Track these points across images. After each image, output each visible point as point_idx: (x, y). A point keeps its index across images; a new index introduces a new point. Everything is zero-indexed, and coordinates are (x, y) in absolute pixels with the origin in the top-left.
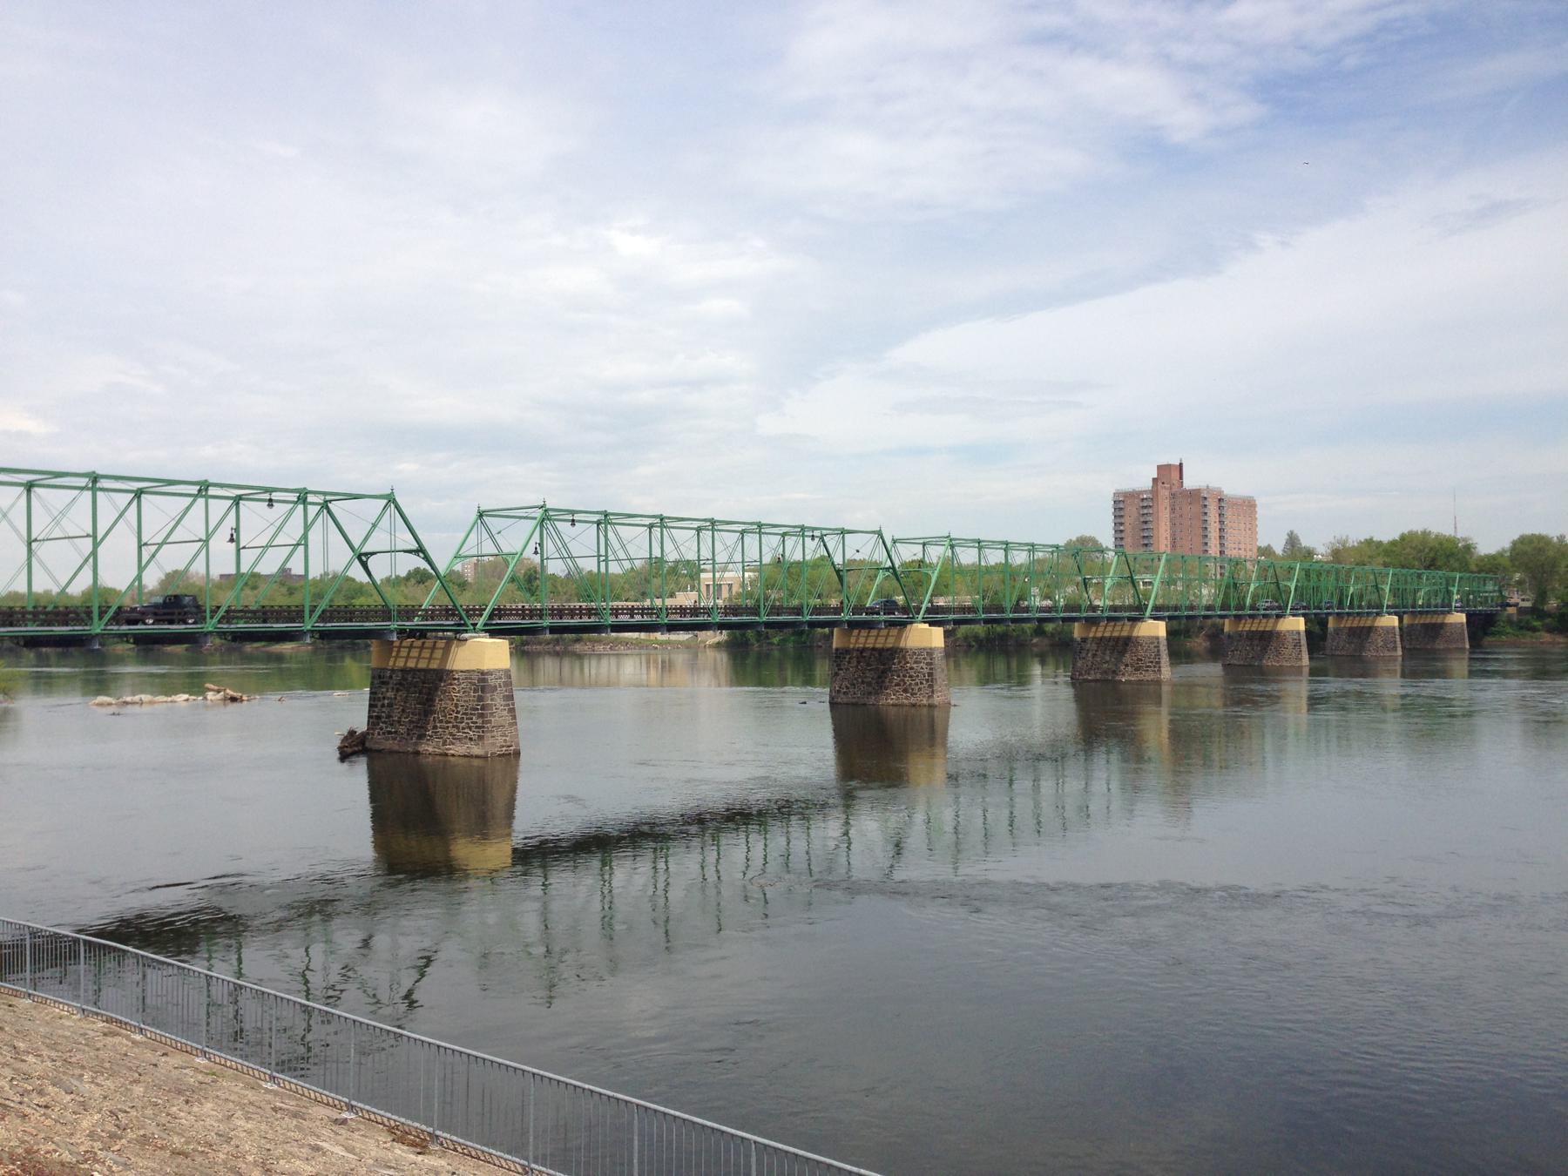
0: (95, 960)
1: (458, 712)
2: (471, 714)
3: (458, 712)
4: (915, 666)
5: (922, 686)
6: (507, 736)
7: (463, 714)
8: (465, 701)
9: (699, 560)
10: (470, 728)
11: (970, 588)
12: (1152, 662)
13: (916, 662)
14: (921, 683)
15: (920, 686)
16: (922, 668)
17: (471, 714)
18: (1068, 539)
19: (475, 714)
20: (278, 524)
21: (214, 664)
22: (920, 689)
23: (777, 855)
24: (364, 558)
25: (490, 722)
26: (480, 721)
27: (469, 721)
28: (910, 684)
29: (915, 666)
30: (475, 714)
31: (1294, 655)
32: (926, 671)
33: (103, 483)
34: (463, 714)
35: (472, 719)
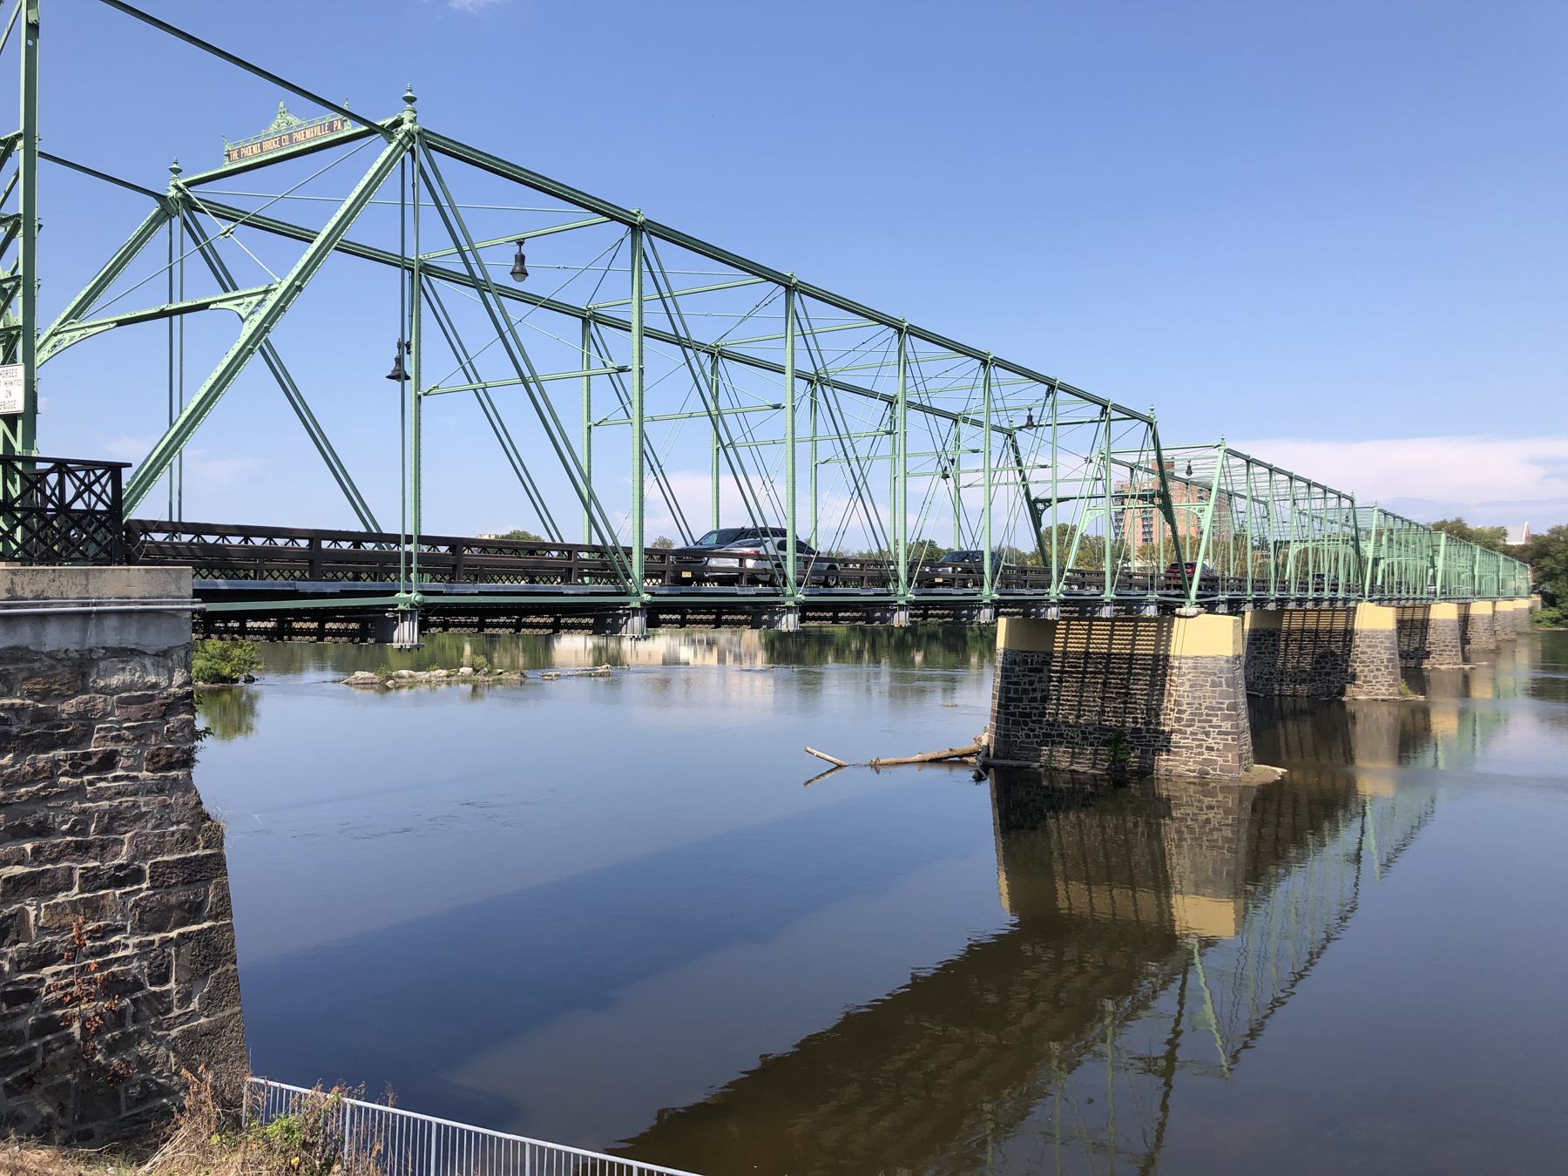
10: (1207, 734)
12: (1447, 646)
13: (1369, 647)
14: (1378, 670)
15: (1377, 673)
17: (1207, 715)
22: (1376, 677)
27: (1206, 725)
29: (1367, 650)
31: (1484, 638)
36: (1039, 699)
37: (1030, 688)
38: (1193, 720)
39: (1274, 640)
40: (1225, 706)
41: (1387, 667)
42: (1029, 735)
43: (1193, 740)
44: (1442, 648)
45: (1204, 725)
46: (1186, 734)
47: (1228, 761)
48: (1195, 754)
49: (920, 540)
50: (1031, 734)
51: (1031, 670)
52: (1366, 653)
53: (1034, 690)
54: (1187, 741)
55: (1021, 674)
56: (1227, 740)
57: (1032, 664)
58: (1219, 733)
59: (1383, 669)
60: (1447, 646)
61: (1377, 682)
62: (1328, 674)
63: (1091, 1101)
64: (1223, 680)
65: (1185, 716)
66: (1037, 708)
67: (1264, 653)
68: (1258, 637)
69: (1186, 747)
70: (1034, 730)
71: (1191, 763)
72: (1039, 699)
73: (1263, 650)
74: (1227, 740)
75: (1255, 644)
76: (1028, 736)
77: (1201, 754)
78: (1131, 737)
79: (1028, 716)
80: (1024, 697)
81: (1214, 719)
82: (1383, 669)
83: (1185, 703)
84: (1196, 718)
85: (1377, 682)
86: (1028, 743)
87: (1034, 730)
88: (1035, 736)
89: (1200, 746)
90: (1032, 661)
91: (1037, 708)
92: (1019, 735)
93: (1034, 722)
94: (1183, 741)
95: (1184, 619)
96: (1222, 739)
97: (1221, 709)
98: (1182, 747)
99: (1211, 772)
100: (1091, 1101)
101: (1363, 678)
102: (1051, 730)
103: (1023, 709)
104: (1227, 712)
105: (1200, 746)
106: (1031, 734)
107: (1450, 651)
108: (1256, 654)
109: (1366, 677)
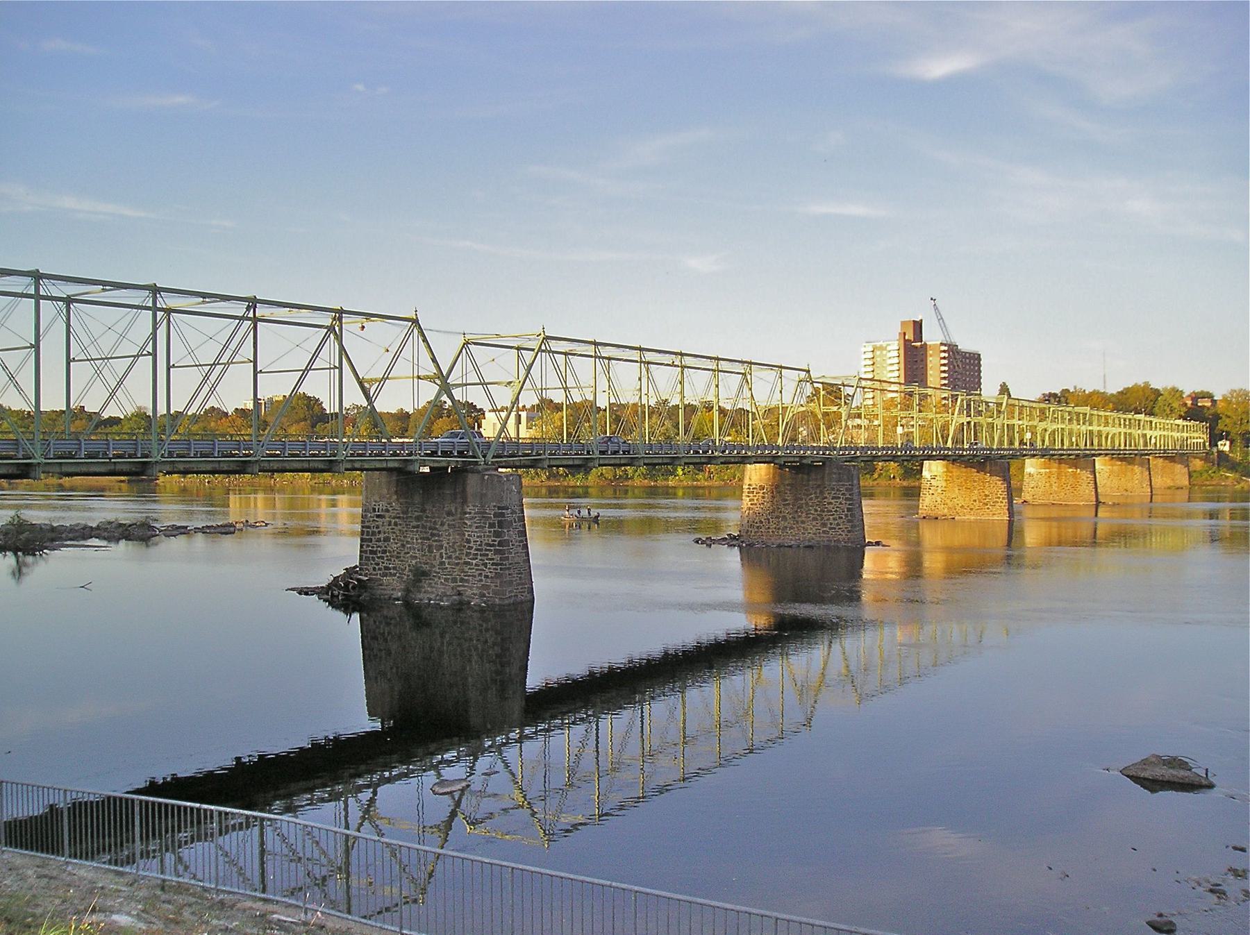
0: (161, 839)
1: (470, 548)
2: (486, 550)
3: (470, 548)
4: (833, 501)
5: (842, 520)
6: (522, 573)
7: (477, 550)
8: (478, 537)
9: (1076, 391)
10: (485, 565)
11: (548, 441)
12: (999, 498)
15: (839, 521)
16: (841, 503)
17: (486, 550)
18: (1135, 382)
19: (491, 550)
20: (393, 350)
21: (165, 502)
23: (212, 845)
24: (367, 385)
25: (507, 558)
26: (497, 557)
27: (485, 558)
28: (828, 519)
29: (833, 501)
30: (491, 550)
31: (1087, 491)
32: (845, 507)
33: (261, 311)
34: (477, 550)
35: (488, 555)
36: (382, 539)
37: (377, 530)
38: (477, 554)
39: (763, 493)
40: (496, 543)
41: (846, 516)
42: (375, 568)
43: (477, 570)
44: (995, 500)
45: (483, 558)
46: (472, 565)
47: (497, 586)
48: (477, 581)
49: (172, 412)
50: (377, 567)
51: (378, 516)
52: (831, 503)
53: (379, 532)
54: (472, 571)
55: (371, 519)
56: (497, 570)
57: (378, 512)
58: (493, 564)
59: (844, 517)
60: (999, 498)
61: (839, 529)
62: (803, 522)
63: (1155, 870)
64: (496, 522)
65: (473, 551)
66: (381, 547)
67: (756, 504)
68: (752, 490)
69: (472, 576)
70: (378, 564)
71: (475, 589)
72: (382, 539)
73: (755, 502)
74: (497, 570)
75: (749, 496)
76: (374, 569)
77: (481, 580)
78: (439, 568)
79: (374, 552)
80: (373, 538)
81: (490, 553)
82: (844, 517)
83: (472, 541)
84: (479, 553)
85: (839, 529)
86: (374, 575)
87: (378, 564)
88: (380, 569)
89: (480, 574)
90: (379, 509)
91: (381, 547)
92: (369, 568)
93: (378, 558)
94: (470, 571)
95: (1099, 497)
96: (495, 569)
97: (493, 545)
98: (469, 576)
99: (487, 595)
100: (1155, 870)
101: (829, 526)
102: (390, 564)
103: (372, 547)
104: (497, 548)
105: (480, 574)
106: (377, 567)
107: (1002, 502)
108: (749, 506)
109: (831, 524)
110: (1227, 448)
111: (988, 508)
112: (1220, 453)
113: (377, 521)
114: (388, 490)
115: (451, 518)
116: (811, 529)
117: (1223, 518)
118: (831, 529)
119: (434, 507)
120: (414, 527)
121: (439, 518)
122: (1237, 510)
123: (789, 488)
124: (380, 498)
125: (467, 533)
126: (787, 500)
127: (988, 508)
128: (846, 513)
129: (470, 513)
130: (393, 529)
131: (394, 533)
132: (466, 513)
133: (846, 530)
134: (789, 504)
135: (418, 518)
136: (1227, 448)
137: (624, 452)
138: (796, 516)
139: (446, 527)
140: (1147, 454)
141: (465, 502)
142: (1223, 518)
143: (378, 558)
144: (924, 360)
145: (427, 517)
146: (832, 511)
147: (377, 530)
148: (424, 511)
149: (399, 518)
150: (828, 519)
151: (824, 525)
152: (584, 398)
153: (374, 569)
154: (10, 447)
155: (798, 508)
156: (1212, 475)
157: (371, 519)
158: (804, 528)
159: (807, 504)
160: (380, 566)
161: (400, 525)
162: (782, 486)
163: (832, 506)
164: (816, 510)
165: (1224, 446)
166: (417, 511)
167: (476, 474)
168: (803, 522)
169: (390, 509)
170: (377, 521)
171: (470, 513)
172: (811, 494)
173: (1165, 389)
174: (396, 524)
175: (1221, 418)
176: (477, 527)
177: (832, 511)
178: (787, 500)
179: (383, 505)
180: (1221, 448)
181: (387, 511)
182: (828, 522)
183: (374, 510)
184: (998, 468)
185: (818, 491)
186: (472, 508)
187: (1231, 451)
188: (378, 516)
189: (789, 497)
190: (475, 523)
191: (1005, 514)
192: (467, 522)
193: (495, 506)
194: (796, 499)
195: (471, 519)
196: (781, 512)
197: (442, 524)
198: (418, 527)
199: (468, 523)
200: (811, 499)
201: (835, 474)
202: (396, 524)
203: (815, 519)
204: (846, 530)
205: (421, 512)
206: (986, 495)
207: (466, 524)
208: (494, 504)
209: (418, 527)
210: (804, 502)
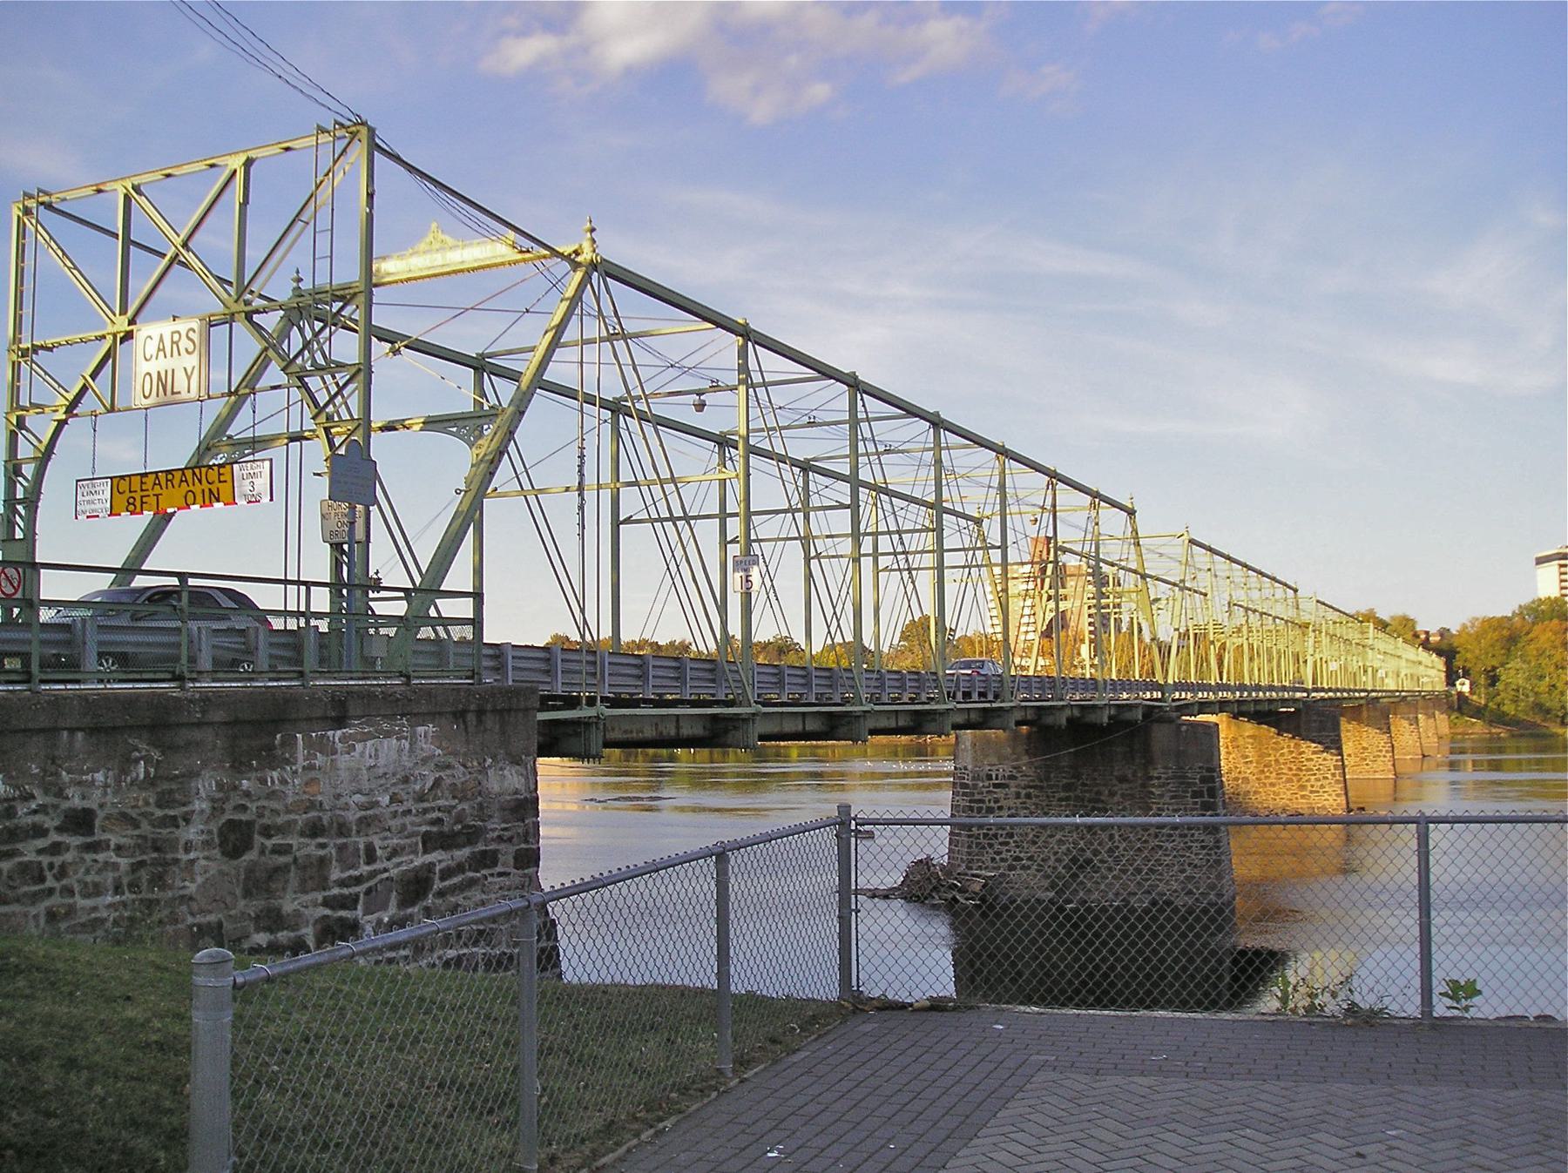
4: (1313, 757)
5: (1328, 781)
12: (1381, 751)
28: (1308, 781)
29: (1313, 757)
50: (998, 858)
51: (995, 786)
55: (985, 790)
57: (997, 779)
60: (1381, 751)
62: (1272, 785)
64: (1205, 789)
76: (993, 859)
87: (998, 853)
90: (997, 775)
101: (1309, 788)
106: (998, 858)
107: (1385, 756)
109: (1312, 786)
110: (1466, 689)
111: (1367, 765)
112: (1460, 694)
113: (995, 793)
114: (1014, 749)
115: (1125, 786)
116: (1285, 793)
117: (1465, 770)
118: (1311, 792)
119: (1095, 770)
120: (1060, 800)
121: (1104, 785)
122: (863, 776)
123: (1251, 741)
124: (999, 759)
125: (1154, 806)
126: (1247, 757)
127: (1367, 765)
128: (1333, 771)
129: (1159, 778)
130: (1024, 803)
131: (1026, 808)
132: (1151, 778)
133: (1334, 794)
134: (1251, 762)
135: (1067, 787)
136: (1466, 689)
137: (982, 694)
138: (1263, 776)
139: (1117, 798)
140: (1204, 707)
141: (1149, 762)
142: (1465, 770)
143: (1001, 844)
144: (1541, 558)
145: (1084, 785)
146: (1312, 770)
147: (996, 806)
148: (1077, 776)
149: (1031, 787)
150: (1308, 781)
151: (1303, 787)
152: (735, 629)
153: (993, 859)
154: (701, 674)
155: (1265, 766)
156: (1456, 721)
157: (985, 790)
158: (1274, 793)
159: (1277, 761)
160: (1003, 856)
161: (1037, 797)
162: (1240, 739)
163: (1313, 763)
164: (1290, 769)
165: (1463, 686)
166: (1064, 778)
167: (1166, 725)
168: (1272, 785)
169: (1018, 775)
170: (995, 793)
171: (1159, 778)
172: (1283, 748)
173: (1393, 618)
174: (1028, 796)
175: (1459, 652)
176: (1172, 798)
177: (1312, 770)
178: (1247, 757)
179: (1004, 769)
180: (1459, 687)
181: (1012, 777)
182: (1308, 784)
183: (989, 777)
184: (1378, 714)
185: (1292, 745)
186: (1162, 771)
187: (1472, 692)
188: (995, 786)
189: (1251, 753)
190: (1170, 791)
191: (1389, 771)
192: (1153, 790)
193: (1200, 768)
194: (1261, 756)
195: (1160, 786)
196: (1240, 773)
197: (1112, 794)
198: (1067, 798)
199: (1157, 791)
200: (1282, 755)
201: (1315, 721)
202: (1028, 796)
203: (1289, 780)
204: (1334, 794)
205: (1073, 777)
206: (1364, 748)
207: (1153, 793)
208: (1201, 765)
209: (1067, 798)
210: (1272, 758)
